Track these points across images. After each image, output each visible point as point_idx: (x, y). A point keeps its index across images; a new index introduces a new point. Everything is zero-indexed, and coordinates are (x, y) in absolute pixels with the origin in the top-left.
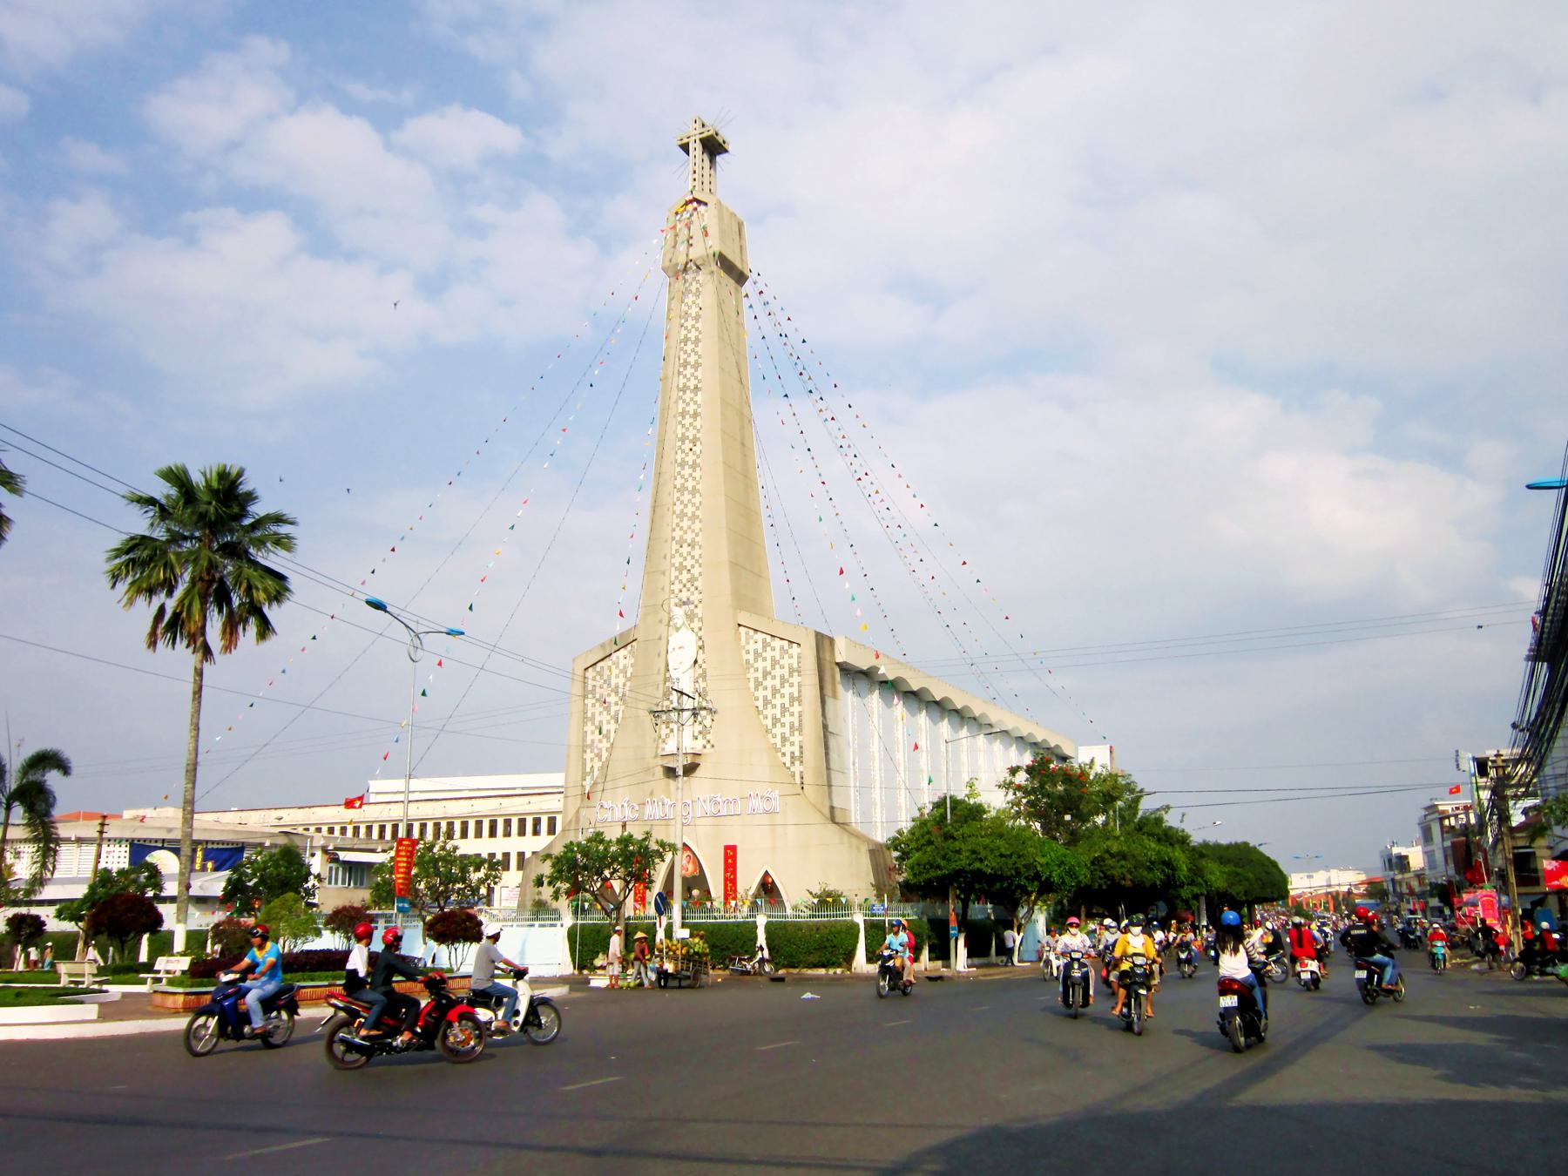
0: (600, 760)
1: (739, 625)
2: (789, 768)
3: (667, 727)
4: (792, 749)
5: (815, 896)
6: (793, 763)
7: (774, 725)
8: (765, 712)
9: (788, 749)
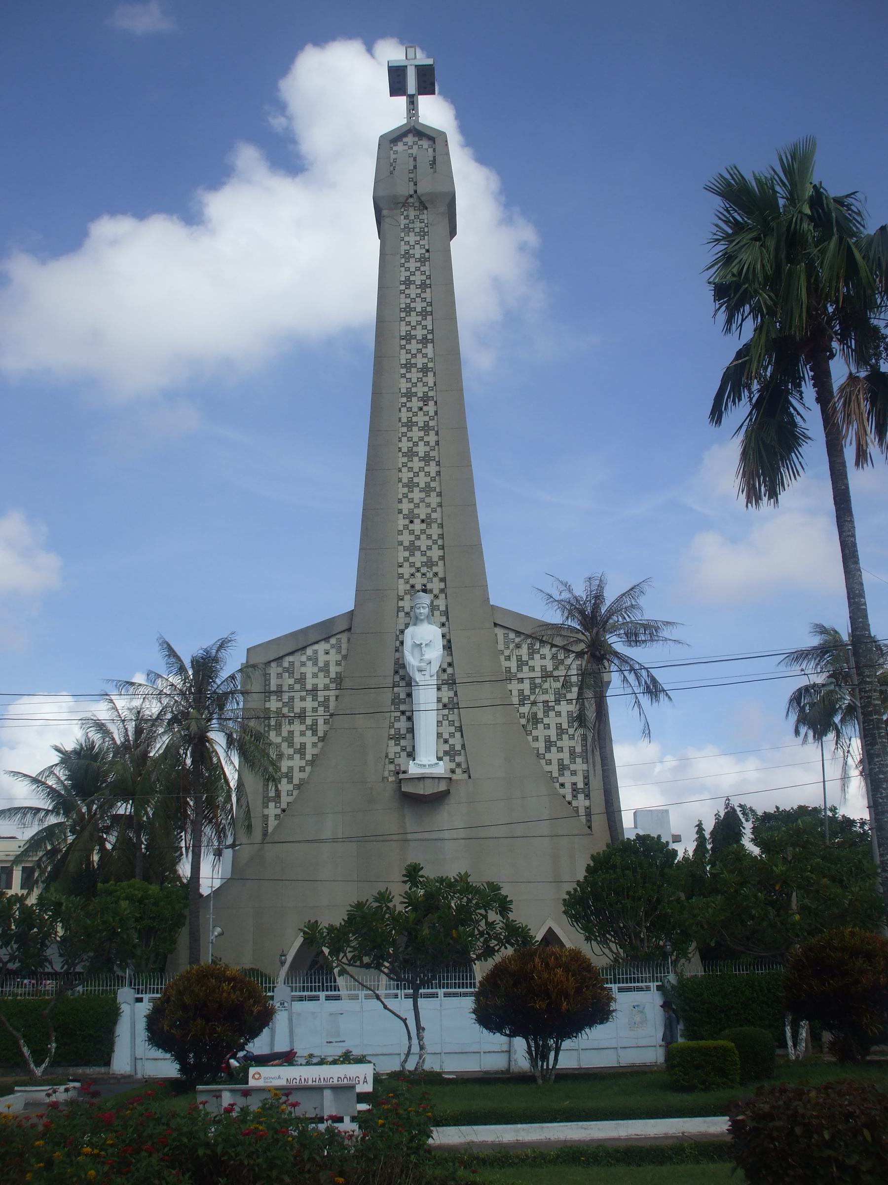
0: (339, 652)
1: (496, 625)
2: (570, 803)
3: (396, 745)
4: (574, 779)
5: (613, 1011)
6: (575, 797)
7: (548, 749)
8: (535, 733)
9: (567, 779)
